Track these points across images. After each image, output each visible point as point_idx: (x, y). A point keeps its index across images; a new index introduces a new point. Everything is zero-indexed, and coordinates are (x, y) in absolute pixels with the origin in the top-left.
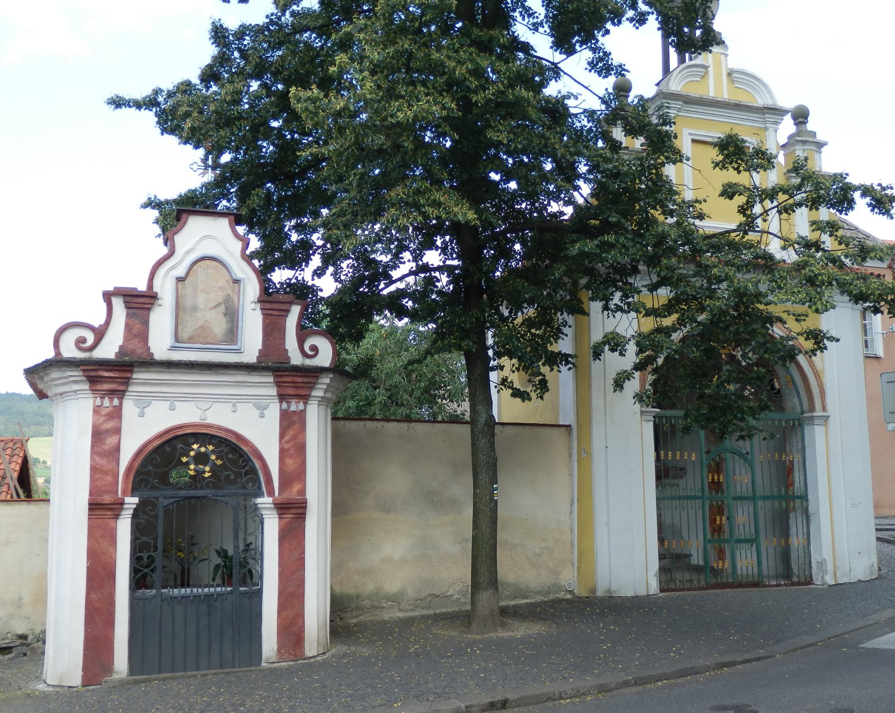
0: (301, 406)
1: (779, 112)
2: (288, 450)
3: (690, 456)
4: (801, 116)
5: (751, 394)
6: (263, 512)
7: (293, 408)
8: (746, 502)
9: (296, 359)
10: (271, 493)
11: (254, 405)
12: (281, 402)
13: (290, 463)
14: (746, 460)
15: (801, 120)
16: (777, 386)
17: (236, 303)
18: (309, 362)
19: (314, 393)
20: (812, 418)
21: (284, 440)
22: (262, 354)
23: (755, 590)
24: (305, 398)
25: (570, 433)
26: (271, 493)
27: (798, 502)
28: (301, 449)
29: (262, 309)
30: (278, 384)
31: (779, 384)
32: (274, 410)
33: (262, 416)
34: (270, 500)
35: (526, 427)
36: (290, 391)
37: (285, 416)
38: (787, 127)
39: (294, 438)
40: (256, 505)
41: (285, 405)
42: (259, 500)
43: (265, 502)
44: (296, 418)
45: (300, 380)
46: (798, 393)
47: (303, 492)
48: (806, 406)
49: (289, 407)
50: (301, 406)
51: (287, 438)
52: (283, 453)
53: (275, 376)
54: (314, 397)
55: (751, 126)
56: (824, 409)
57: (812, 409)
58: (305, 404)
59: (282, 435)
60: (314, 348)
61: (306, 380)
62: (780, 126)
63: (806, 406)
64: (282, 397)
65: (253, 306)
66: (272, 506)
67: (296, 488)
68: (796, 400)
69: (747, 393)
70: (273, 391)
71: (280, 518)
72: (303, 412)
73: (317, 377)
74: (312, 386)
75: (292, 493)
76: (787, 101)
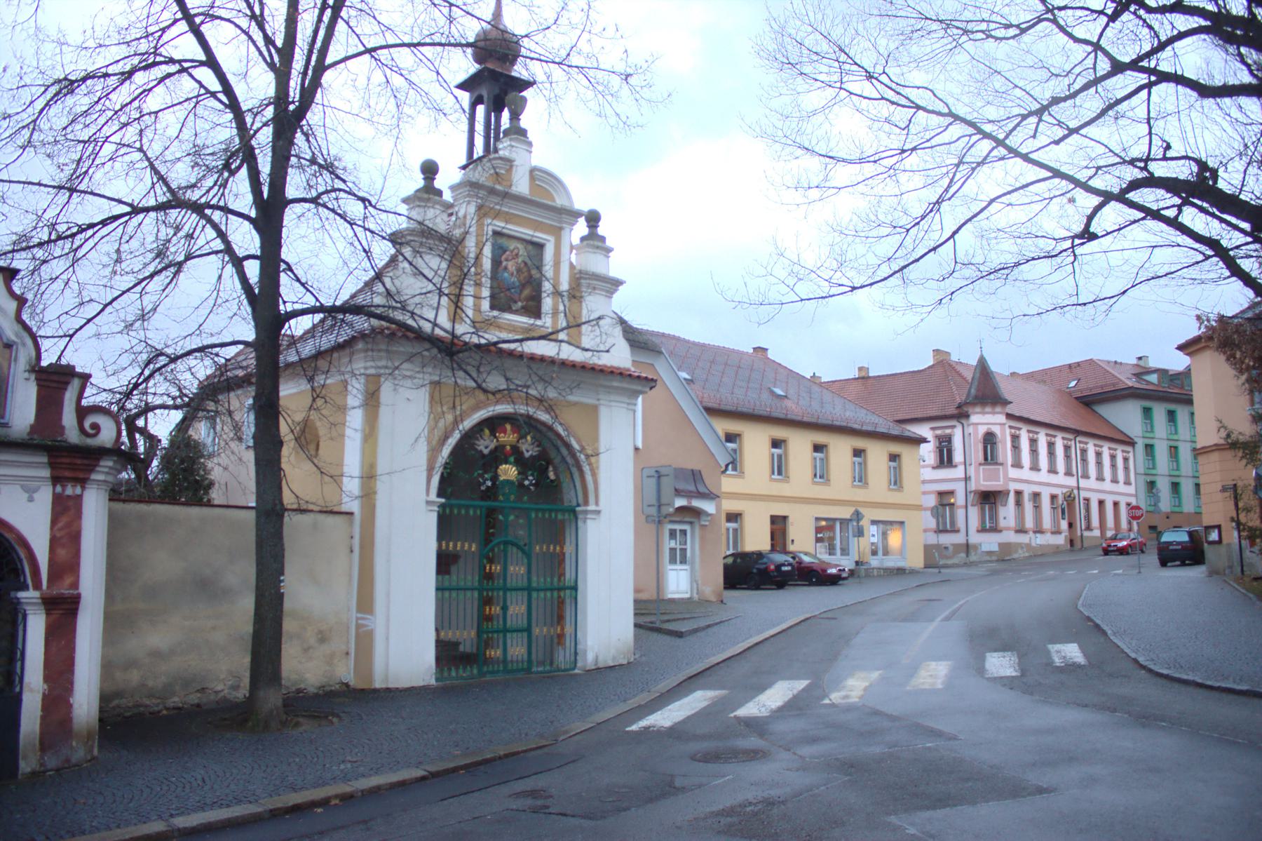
0: (78, 491)
1: (576, 215)
2: (61, 537)
3: (470, 547)
4: (593, 219)
5: (531, 484)
6: (28, 608)
7: (69, 491)
8: (520, 593)
9: (72, 435)
10: (38, 586)
11: (22, 487)
12: (54, 486)
13: (62, 553)
14: (524, 552)
15: (592, 223)
16: (552, 475)
17: (6, 370)
18: (90, 442)
19: (94, 476)
20: (586, 512)
21: (56, 528)
22: (33, 429)
23: (1064, 169)
24: (83, 482)
25: (351, 523)
26: (38, 586)
27: (568, 592)
28: (75, 538)
29: (37, 379)
30: (52, 465)
31: (556, 474)
32: (45, 496)
33: (31, 500)
34: (37, 594)
35: (655, 546)
36: (67, 474)
37: (58, 502)
38: (581, 228)
39: (69, 525)
40: (18, 599)
41: (59, 489)
42: (21, 594)
43: (29, 596)
44: (71, 503)
45: (79, 461)
46: (575, 486)
47: (76, 585)
48: (581, 500)
49: (64, 490)
50: (78, 491)
51: (60, 525)
52: (54, 542)
53: (50, 457)
54: (94, 480)
55: (551, 225)
56: (597, 504)
57: (586, 503)
58: (83, 488)
59: (54, 522)
60: (96, 427)
61: (86, 462)
62: (574, 227)
63: (581, 500)
64: (55, 480)
65: (26, 375)
66: (40, 601)
67: (68, 580)
68: (573, 493)
69: (526, 483)
70: (46, 473)
71: (47, 614)
72: (80, 497)
73: (98, 460)
74: (91, 469)
75: (64, 589)
76: (581, 203)
